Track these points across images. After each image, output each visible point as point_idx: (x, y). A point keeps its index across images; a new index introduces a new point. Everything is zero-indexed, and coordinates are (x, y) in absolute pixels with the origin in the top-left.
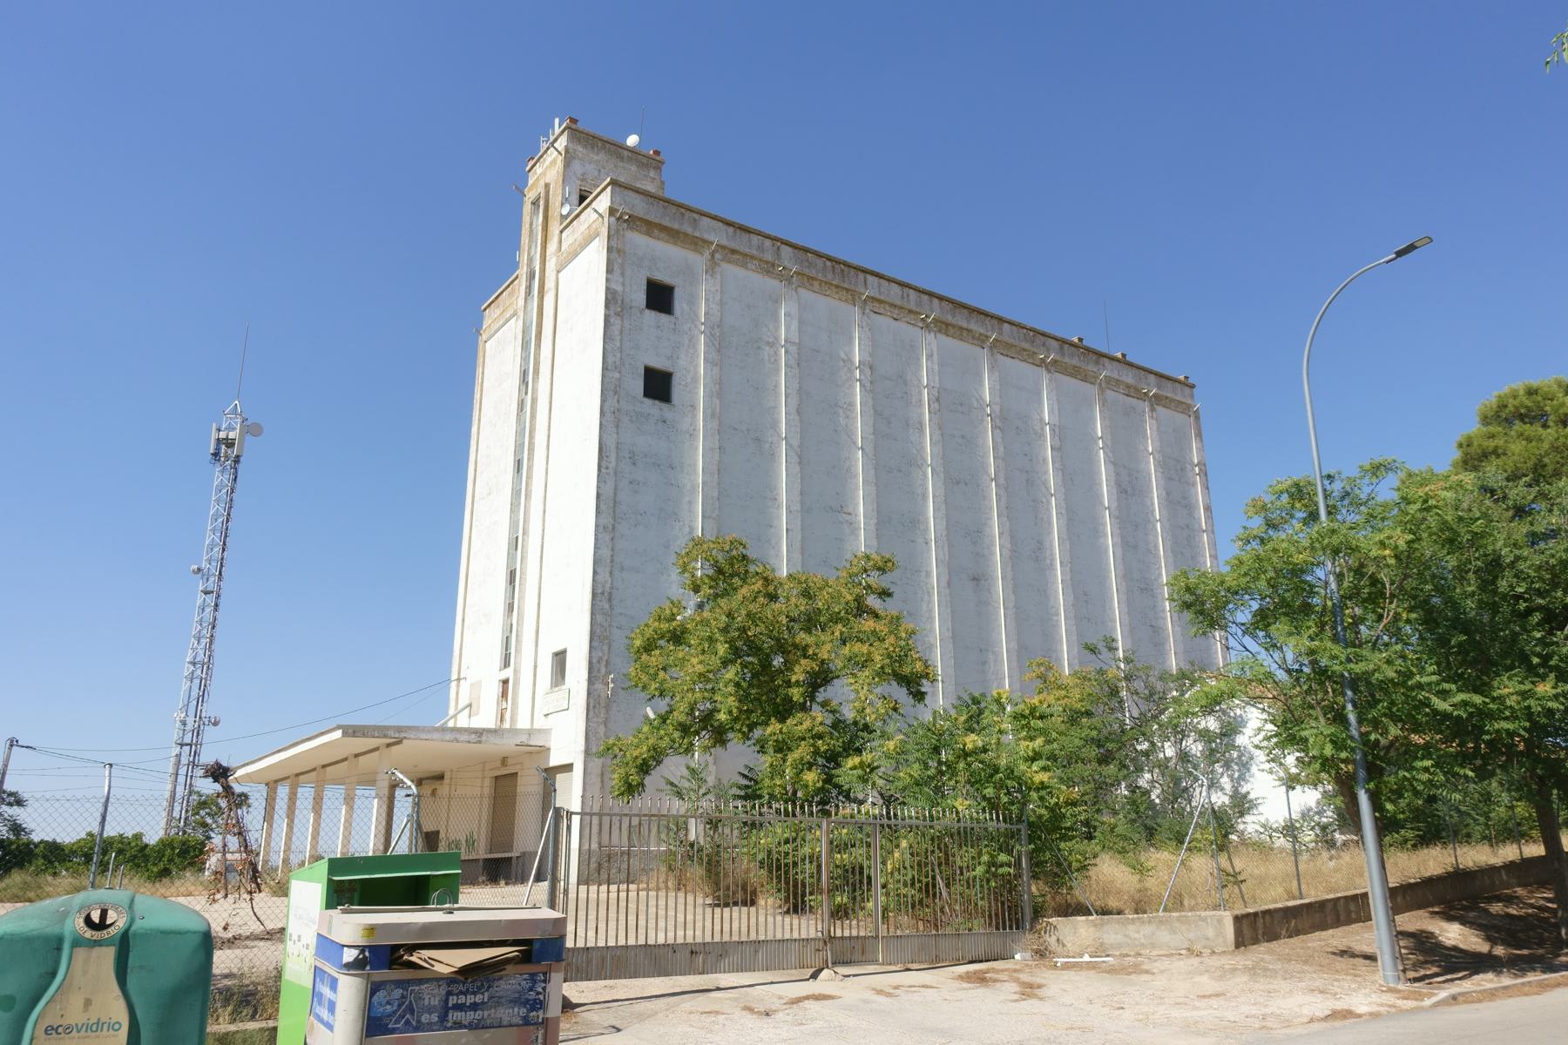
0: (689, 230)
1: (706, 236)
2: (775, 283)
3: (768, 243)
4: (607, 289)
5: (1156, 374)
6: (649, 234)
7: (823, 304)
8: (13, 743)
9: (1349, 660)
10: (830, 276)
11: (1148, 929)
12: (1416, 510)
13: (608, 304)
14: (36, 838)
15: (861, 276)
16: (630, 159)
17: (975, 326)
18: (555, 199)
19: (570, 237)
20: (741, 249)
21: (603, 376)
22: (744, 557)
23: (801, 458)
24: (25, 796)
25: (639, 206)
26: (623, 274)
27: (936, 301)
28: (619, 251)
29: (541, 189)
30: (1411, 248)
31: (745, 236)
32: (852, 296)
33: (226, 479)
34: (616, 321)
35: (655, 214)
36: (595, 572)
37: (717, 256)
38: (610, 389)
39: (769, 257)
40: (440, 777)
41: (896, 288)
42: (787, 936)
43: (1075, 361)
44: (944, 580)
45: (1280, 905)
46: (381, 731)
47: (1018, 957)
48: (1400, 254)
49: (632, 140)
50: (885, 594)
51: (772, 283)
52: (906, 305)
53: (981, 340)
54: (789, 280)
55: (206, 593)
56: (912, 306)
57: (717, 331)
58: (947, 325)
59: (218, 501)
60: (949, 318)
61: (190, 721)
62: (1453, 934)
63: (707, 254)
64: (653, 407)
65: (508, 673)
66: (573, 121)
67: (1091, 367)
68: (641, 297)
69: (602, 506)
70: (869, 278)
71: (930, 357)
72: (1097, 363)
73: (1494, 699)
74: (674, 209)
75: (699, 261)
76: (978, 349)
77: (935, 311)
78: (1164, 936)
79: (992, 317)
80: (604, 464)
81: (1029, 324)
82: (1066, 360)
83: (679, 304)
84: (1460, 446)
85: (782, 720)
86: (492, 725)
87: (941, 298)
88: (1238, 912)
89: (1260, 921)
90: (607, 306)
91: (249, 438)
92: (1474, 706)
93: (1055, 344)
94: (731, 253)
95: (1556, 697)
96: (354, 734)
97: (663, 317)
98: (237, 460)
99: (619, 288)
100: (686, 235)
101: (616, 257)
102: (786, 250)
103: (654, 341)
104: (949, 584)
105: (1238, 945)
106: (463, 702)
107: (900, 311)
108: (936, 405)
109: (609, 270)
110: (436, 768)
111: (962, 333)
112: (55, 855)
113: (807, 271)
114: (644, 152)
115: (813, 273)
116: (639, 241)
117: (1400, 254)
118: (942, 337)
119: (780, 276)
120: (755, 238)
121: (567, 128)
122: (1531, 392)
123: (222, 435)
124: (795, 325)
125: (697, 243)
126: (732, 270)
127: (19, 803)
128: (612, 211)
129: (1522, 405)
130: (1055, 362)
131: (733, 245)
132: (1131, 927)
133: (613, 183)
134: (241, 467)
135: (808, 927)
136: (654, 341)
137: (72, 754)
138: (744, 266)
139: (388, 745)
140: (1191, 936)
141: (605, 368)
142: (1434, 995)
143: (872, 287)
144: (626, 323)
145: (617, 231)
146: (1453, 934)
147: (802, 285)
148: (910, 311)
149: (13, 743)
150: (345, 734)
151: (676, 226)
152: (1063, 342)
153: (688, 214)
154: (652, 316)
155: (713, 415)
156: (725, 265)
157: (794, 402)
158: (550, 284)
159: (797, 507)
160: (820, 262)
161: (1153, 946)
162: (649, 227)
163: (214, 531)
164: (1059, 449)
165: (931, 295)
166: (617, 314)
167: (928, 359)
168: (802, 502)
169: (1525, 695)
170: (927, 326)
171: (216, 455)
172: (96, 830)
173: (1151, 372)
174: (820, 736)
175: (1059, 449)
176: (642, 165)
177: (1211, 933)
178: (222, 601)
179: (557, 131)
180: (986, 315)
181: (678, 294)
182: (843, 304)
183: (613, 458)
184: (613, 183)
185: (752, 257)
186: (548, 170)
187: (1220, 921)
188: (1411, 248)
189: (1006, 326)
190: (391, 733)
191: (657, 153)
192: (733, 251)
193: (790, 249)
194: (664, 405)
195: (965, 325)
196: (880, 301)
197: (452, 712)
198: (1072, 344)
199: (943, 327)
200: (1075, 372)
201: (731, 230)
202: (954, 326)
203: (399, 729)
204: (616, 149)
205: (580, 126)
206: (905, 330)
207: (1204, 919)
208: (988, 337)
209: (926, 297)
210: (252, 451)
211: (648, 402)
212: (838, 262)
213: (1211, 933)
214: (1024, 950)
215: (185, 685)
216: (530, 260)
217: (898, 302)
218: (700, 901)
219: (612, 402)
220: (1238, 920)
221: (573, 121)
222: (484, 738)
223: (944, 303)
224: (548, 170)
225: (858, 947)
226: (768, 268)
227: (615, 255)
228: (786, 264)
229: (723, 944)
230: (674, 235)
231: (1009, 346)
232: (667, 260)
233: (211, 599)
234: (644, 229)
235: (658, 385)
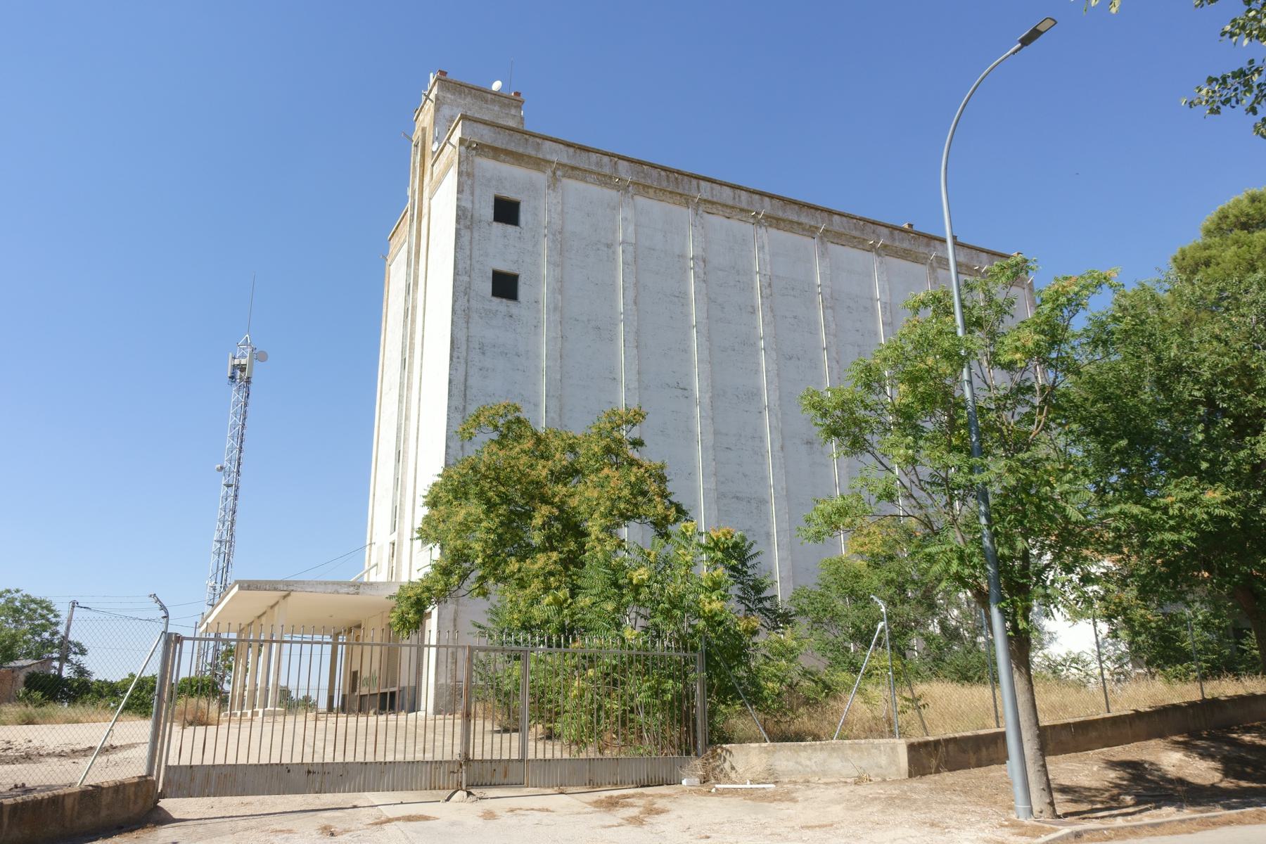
0: (533, 153)
1: (548, 157)
2: (613, 193)
3: (606, 159)
4: (458, 207)
5: (988, 252)
6: (495, 158)
7: (656, 209)
8: (74, 604)
9: (972, 470)
10: (664, 184)
11: (820, 756)
12: (1131, 330)
13: (458, 219)
14: (94, 678)
15: (694, 182)
16: (493, 101)
17: (805, 219)
18: (429, 138)
19: (438, 168)
20: (581, 166)
21: (455, 280)
22: (519, 420)
23: (638, 342)
24: (86, 645)
25: (487, 135)
26: (472, 194)
27: (767, 199)
28: (468, 175)
29: (419, 133)
30: (1035, 34)
31: (584, 154)
32: (686, 200)
33: (241, 397)
34: (466, 234)
35: (501, 141)
36: (447, 447)
37: (559, 173)
38: (461, 290)
39: (607, 171)
40: (359, 626)
41: (727, 191)
42: (419, 757)
43: (906, 245)
44: (777, 445)
45: (969, 734)
46: (272, 586)
47: (684, 782)
48: (1025, 42)
49: (496, 86)
50: (637, 443)
51: (610, 194)
52: (738, 205)
53: (811, 231)
54: (626, 189)
55: (229, 486)
56: (744, 205)
57: (558, 237)
58: (778, 219)
59: (235, 414)
60: (780, 214)
61: (218, 586)
62: (1172, 760)
63: (549, 172)
64: (501, 304)
65: (394, 537)
66: (443, 73)
67: (922, 249)
68: (488, 211)
69: (455, 391)
70: (702, 183)
71: (761, 248)
72: (928, 245)
73: (1154, 510)
74: (518, 136)
75: (540, 178)
76: (810, 240)
77: (767, 207)
78: (836, 764)
79: (823, 210)
80: (455, 354)
81: (859, 215)
82: (897, 244)
83: (524, 217)
84: (1175, 260)
85: (522, 559)
86: (385, 580)
87: (772, 197)
88: (918, 738)
89: (942, 750)
90: (458, 221)
91: (257, 364)
92: (1134, 517)
93: (885, 231)
94: (573, 171)
95: (1228, 503)
96: (249, 588)
97: (510, 228)
98: (248, 381)
99: (469, 205)
100: (530, 157)
101: (466, 176)
102: (623, 165)
103: (503, 249)
104: (782, 448)
105: (910, 776)
106: (373, 563)
107: (730, 210)
108: (768, 291)
109: (460, 191)
110: (352, 617)
111: (792, 226)
112: (107, 692)
113: (642, 181)
114: (506, 93)
115: (649, 182)
116: (486, 164)
117: (1025, 42)
118: (773, 231)
119: (617, 187)
120: (594, 157)
121: (438, 79)
122: (1254, 199)
123: (236, 362)
124: (631, 228)
125: (538, 163)
126: (572, 186)
127: (83, 652)
128: (462, 141)
129: (1242, 213)
130: (885, 246)
131: (573, 163)
132: (803, 754)
133: (464, 117)
134: (252, 387)
135: (554, 751)
136: (503, 249)
137: (128, 614)
138: (584, 180)
139: (285, 597)
140: (864, 764)
141: (456, 273)
142: (1056, 831)
143: (706, 190)
144: (476, 235)
145: (467, 157)
146: (1172, 760)
147: (639, 194)
148: (742, 210)
149: (74, 604)
150: (241, 588)
151: (521, 150)
152: (894, 228)
153: (531, 139)
154: (499, 227)
155: (555, 309)
156: (565, 180)
157: (631, 294)
158: (425, 211)
159: (634, 385)
160: (655, 172)
161: (825, 773)
162: (496, 152)
163: (232, 437)
164: (891, 324)
165: (762, 194)
166: (468, 227)
167: (763, 250)
168: (639, 381)
169: (1193, 502)
170: (759, 222)
171: (233, 377)
172: (154, 669)
173: (982, 251)
174: (551, 574)
175: (891, 324)
176: (503, 105)
177: (883, 760)
178: (240, 492)
179: (432, 81)
180: (816, 208)
181: (522, 208)
182: (676, 207)
183: (464, 347)
184: (464, 117)
185: (591, 172)
186: (426, 118)
187: (893, 749)
188: (1035, 34)
189: (836, 217)
190: (281, 587)
191: (517, 94)
192: (573, 168)
193: (626, 163)
194: (511, 303)
195: (795, 218)
196: (713, 203)
197: (367, 567)
198: (902, 230)
199: (774, 221)
200: (905, 255)
201: (571, 150)
202: (784, 220)
203: (287, 583)
204: (481, 93)
205: (449, 77)
206: (738, 227)
207: (877, 747)
208: (817, 228)
209: (757, 197)
210: (259, 373)
211: (497, 300)
212: (672, 171)
213: (883, 760)
214: (689, 776)
215: (214, 559)
216: (414, 192)
217: (730, 203)
218: (488, 726)
219: (463, 301)
220: (912, 748)
221: (443, 73)
222: (361, 590)
223: (775, 202)
224: (426, 118)
225: (500, 769)
226: (605, 180)
227: (465, 178)
228: (624, 176)
229: (345, 764)
230: (518, 158)
231: (839, 235)
232: (512, 179)
233: (231, 492)
234: (491, 154)
235: (505, 286)
